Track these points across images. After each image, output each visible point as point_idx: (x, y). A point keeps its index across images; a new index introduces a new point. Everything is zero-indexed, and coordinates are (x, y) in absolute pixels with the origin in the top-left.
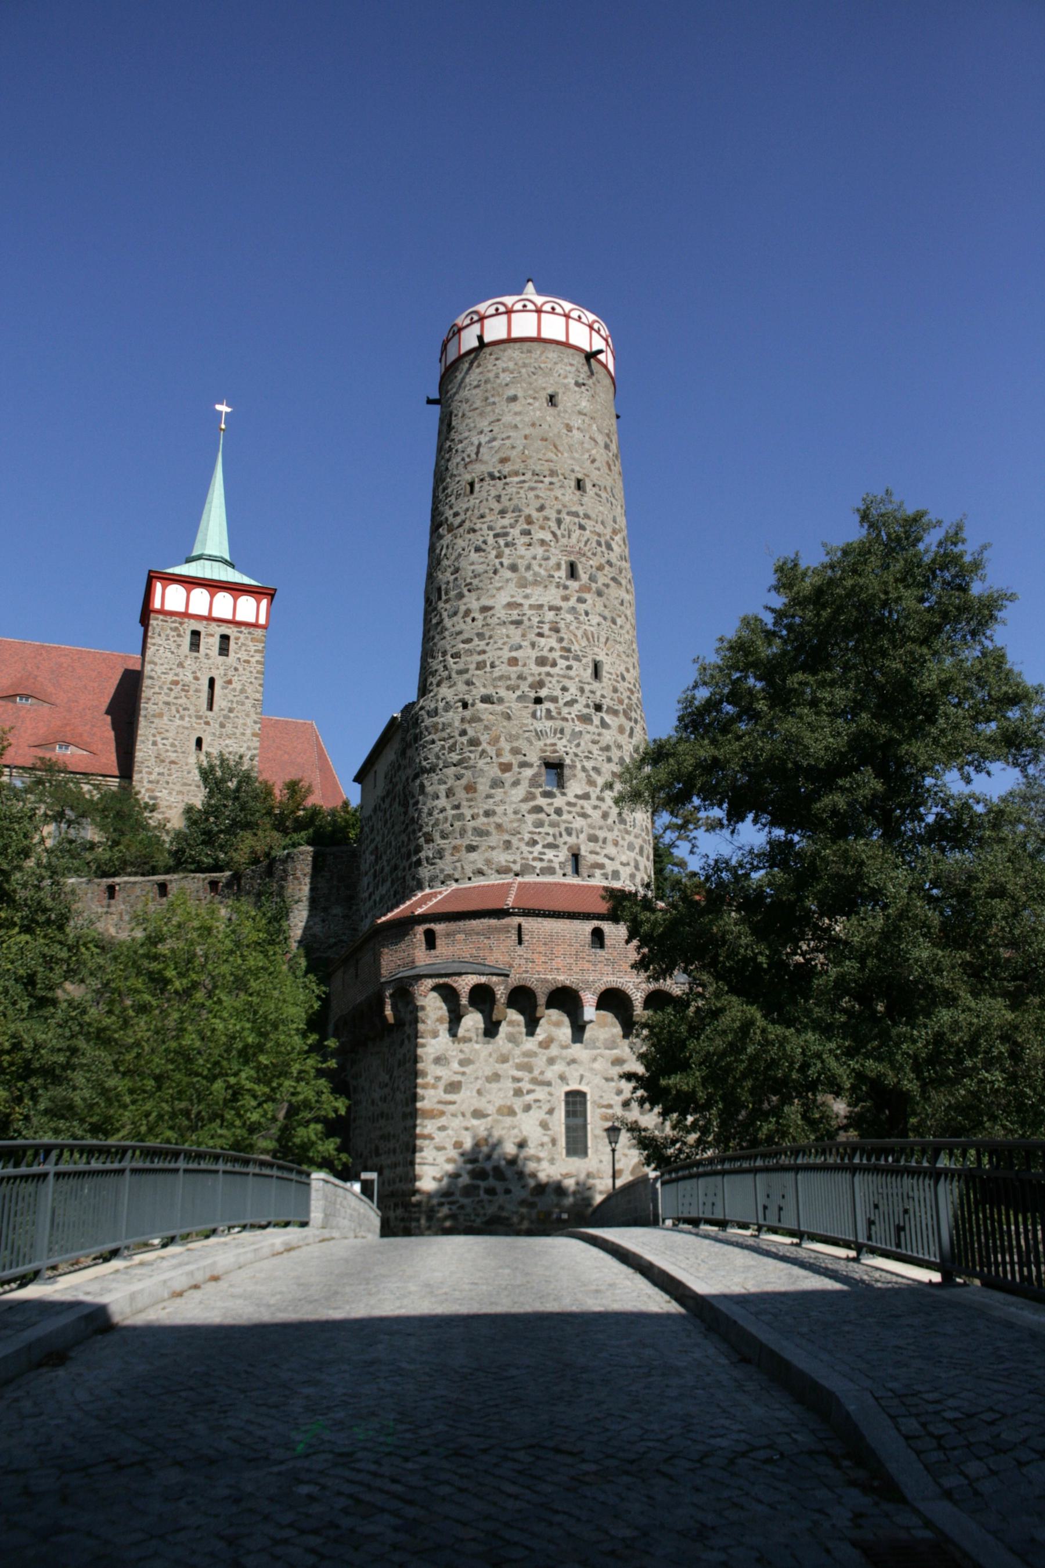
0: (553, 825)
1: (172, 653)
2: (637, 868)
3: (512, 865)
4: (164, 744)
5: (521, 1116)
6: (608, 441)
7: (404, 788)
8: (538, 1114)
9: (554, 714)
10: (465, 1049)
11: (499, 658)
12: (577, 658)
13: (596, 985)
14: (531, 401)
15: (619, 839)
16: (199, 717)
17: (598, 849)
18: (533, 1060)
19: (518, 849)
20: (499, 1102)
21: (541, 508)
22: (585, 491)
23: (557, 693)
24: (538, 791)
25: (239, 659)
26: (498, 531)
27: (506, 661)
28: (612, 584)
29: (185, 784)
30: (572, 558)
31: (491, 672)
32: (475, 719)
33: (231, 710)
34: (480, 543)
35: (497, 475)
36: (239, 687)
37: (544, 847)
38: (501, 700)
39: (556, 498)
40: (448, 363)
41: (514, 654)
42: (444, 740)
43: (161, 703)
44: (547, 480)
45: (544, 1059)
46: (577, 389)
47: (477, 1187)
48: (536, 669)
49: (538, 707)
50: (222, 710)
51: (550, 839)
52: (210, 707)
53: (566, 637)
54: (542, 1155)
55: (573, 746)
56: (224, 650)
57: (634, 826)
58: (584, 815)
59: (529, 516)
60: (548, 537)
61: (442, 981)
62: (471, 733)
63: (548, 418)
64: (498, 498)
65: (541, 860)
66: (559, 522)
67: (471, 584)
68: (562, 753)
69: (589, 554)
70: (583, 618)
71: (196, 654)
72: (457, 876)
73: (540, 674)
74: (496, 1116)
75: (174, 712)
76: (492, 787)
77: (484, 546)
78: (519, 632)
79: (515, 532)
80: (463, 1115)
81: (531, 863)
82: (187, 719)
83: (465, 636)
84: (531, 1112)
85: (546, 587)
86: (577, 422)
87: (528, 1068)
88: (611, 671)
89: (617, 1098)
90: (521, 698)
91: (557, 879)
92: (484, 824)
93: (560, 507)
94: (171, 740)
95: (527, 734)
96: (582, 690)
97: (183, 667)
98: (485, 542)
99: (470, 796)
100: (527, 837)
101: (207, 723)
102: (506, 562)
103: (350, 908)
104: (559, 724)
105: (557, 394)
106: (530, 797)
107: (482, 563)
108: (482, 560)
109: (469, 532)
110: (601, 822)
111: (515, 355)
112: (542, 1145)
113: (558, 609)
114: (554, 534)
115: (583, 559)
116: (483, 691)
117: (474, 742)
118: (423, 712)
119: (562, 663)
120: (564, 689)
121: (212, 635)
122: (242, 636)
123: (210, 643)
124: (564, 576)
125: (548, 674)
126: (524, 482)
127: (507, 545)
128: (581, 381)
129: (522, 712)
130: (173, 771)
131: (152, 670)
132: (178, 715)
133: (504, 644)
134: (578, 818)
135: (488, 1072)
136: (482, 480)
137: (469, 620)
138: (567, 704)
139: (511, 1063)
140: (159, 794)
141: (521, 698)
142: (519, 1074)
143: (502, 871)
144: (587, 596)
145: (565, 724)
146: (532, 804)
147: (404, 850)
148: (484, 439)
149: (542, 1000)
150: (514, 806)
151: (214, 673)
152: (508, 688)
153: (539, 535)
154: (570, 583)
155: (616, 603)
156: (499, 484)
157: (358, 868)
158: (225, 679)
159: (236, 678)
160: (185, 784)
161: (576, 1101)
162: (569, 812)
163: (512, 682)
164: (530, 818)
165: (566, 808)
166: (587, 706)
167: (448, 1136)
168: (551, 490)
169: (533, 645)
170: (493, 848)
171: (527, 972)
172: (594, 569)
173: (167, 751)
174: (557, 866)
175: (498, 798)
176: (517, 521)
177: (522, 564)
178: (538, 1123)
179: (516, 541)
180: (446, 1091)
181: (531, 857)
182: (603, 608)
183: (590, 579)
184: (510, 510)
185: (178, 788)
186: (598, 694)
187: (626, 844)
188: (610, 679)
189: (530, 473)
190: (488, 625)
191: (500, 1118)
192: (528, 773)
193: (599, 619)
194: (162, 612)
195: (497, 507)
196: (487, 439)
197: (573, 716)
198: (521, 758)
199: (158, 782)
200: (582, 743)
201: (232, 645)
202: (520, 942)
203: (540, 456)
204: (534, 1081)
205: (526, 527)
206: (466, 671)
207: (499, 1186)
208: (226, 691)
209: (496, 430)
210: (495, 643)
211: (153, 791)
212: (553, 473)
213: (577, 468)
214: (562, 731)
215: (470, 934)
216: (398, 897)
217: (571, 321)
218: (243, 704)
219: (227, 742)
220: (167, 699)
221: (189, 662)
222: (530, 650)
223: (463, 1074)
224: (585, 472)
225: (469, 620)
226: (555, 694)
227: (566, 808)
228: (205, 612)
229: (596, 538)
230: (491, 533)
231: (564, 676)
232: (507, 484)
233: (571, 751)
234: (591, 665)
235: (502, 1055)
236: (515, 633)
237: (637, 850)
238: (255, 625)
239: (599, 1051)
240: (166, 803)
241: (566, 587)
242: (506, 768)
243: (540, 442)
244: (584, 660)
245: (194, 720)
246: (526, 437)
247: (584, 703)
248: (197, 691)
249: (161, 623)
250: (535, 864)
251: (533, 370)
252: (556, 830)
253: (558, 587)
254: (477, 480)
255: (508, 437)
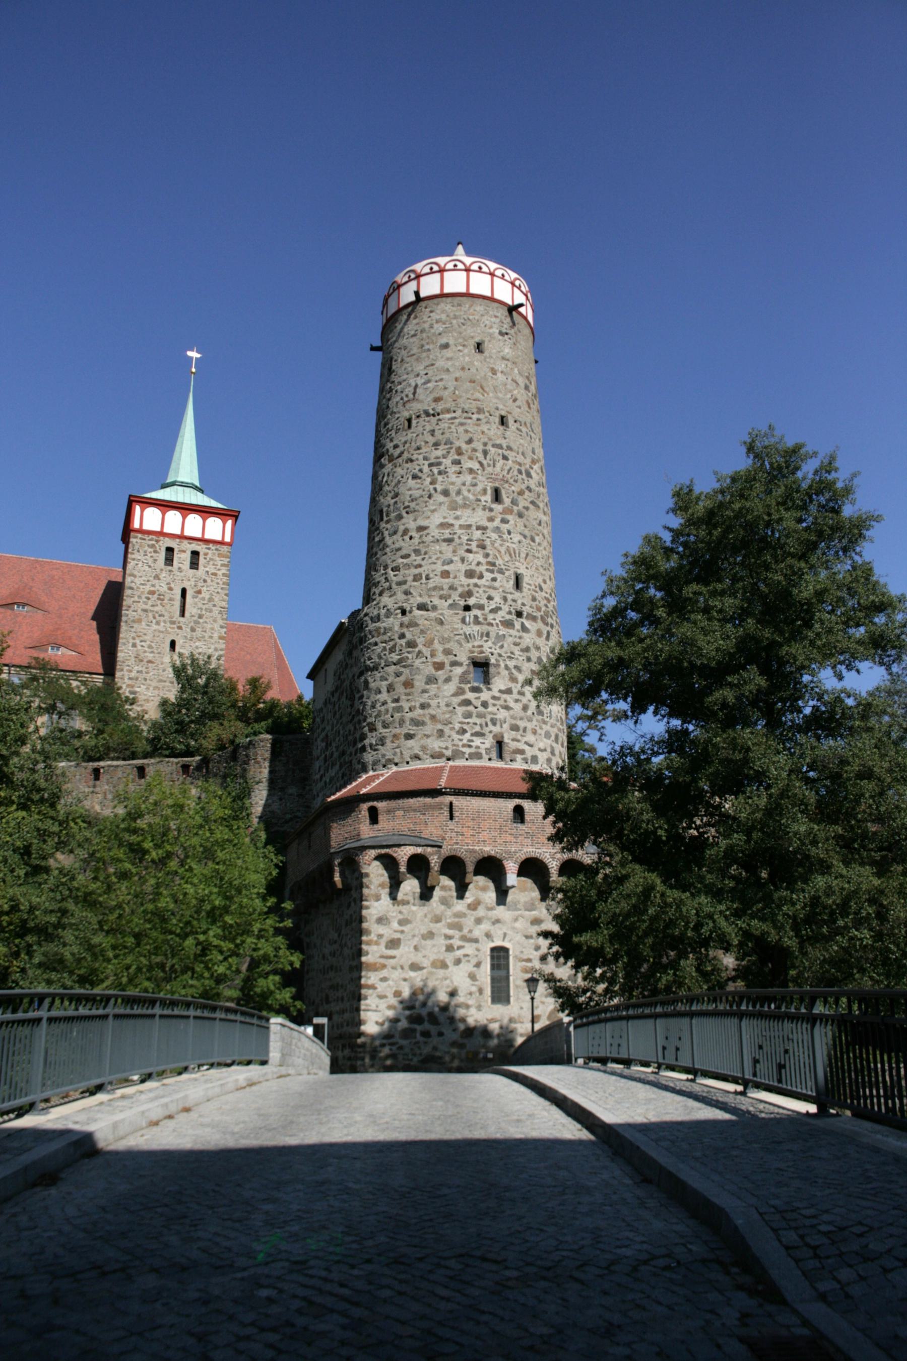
0: (480, 716)
1: (150, 567)
2: (553, 753)
3: (444, 751)
4: (142, 646)
5: (452, 968)
6: (528, 383)
7: (351, 684)
8: (467, 967)
9: (481, 619)
10: (404, 911)
11: (433, 571)
12: (501, 572)
13: (518, 855)
14: (461, 348)
15: (537, 728)
16: (173, 623)
17: (519, 737)
18: (462, 920)
19: (449, 737)
20: (433, 957)
21: (470, 441)
22: (507, 426)
23: (484, 601)
24: (467, 687)
25: (207, 572)
26: (433, 461)
27: (439, 574)
28: (531, 507)
29: (161, 681)
30: (497, 485)
31: (426, 584)
32: (413, 624)
33: (200, 617)
34: (416, 471)
35: (432, 412)
36: (207, 597)
37: (472, 735)
38: (435, 608)
39: (483, 433)
40: (389, 315)
41: (446, 568)
42: (385, 642)
43: (139, 610)
44: (475, 417)
45: (473, 919)
46: (500, 337)
47: (414, 1030)
48: (465, 581)
49: (467, 613)
50: (193, 616)
51: (477, 728)
52: (183, 614)
53: (491, 553)
54: (470, 1002)
55: (497, 647)
56: (194, 565)
57: (551, 717)
58: (507, 708)
59: (459, 448)
60: (476, 466)
61: (383, 851)
62: (409, 636)
63: (476, 363)
64: (432, 432)
65: (470, 746)
66: (485, 453)
67: (408, 507)
68: (487, 654)
69: (511, 481)
70: (506, 536)
71: (170, 568)
72: (396, 761)
73: (468, 585)
74: (430, 969)
75: (151, 618)
76: (427, 683)
77: (420, 474)
78: (451, 548)
79: (447, 462)
80: (402, 968)
81: (461, 749)
82: (162, 624)
83: (404, 552)
84: (461, 965)
85: (474, 509)
86: (500, 366)
87: (458, 927)
88: (530, 582)
89: (535, 953)
90: (452, 606)
91: (484, 763)
92: (420, 715)
93: (486, 440)
94: (148, 643)
95: (457, 637)
96: (505, 599)
97: (159, 579)
98: (421, 471)
99: (408, 691)
100: (457, 726)
101: (180, 628)
102: (439, 488)
103: (304, 788)
104: (485, 628)
105: (483, 342)
106: (460, 692)
107: (419, 489)
108: (418, 486)
109: (407, 462)
110: (522, 714)
111: (447, 308)
112: (471, 994)
113: (484, 529)
114: (481, 464)
115: (506, 485)
116: (420, 600)
117: (412, 644)
118: (367, 618)
119: (488, 576)
120: (490, 598)
121: (184, 551)
122: (210, 552)
123: (182, 558)
124: (489, 500)
125: (476, 585)
126: (455, 418)
127: (440, 473)
128: (504, 331)
129: (453, 618)
130: (150, 669)
131: (132, 582)
132: (154, 621)
133: (437, 559)
134: (502, 710)
135: (424, 930)
136: (418, 417)
137: (407, 538)
138: (492, 611)
139: (443, 922)
140: (138, 689)
141: (452, 606)
142: (450, 932)
143: (436, 756)
144: (509, 517)
145: (490, 628)
146: (462, 697)
147: (350, 738)
148: (420, 381)
149: (470, 868)
150: (446, 699)
151: (186, 585)
152: (441, 597)
153: (468, 464)
154: (494, 506)
155: (535, 523)
156: (433, 420)
157: (311, 754)
158: (196, 589)
159: (205, 589)
160: (161, 681)
161: (500, 956)
162: (494, 705)
163: (445, 592)
164: (460, 710)
165: (491, 701)
166: (510, 613)
167: (389, 986)
168: (478, 425)
169: (463, 560)
170: (428, 736)
171: (457, 843)
172: (516, 494)
173: (145, 652)
174: (483, 752)
175: (432, 693)
176: (448, 452)
177: (453, 490)
178: (467, 975)
179: (448, 470)
180: (387, 947)
181: (461, 743)
182: (523, 528)
183: (512, 502)
184: (443, 442)
185: (154, 684)
186: (519, 602)
187: (543, 733)
188: (529, 590)
189: (460, 411)
190: (423, 542)
191: (434, 970)
192: (459, 671)
193: (520, 537)
194: (141, 531)
195: (431, 440)
196: (423, 381)
197: (497, 621)
198: (452, 658)
199: (137, 679)
200: (505, 645)
201: (202, 560)
202: (451, 817)
203: (469, 396)
204: (464, 938)
205: (456, 457)
206: (405, 582)
207: (433, 1030)
208: (196, 600)
209: (430, 373)
210: (430, 558)
211: (133, 686)
212: (480, 411)
213: (501, 407)
214: (488, 635)
215: (408, 811)
216: (346, 778)
217: (495, 278)
218: (211, 611)
219: (197, 644)
220: (145, 607)
221: (164, 575)
222: (460, 564)
223: (402, 932)
224: (508, 409)
225: (407, 538)
226: (482, 602)
227: (491, 701)
228: (178, 532)
229: (517, 467)
230: (426, 463)
231: (490, 587)
232: (440, 420)
233: (495, 652)
234: (513, 577)
235: (436, 916)
236: (447, 550)
237: (553, 738)
238: (222, 543)
239: (519, 912)
240: (144, 697)
241: (491, 510)
242: (439, 666)
243: (468, 384)
244: (507, 573)
245: (168, 625)
246: (456, 380)
247: (507, 610)
248: (171, 599)
249: (139, 541)
250: (464, 750)
251: (463, 321)
252: (483, 721)
253: (484, 509)
254: (414, 417)
255: (441, 380)
